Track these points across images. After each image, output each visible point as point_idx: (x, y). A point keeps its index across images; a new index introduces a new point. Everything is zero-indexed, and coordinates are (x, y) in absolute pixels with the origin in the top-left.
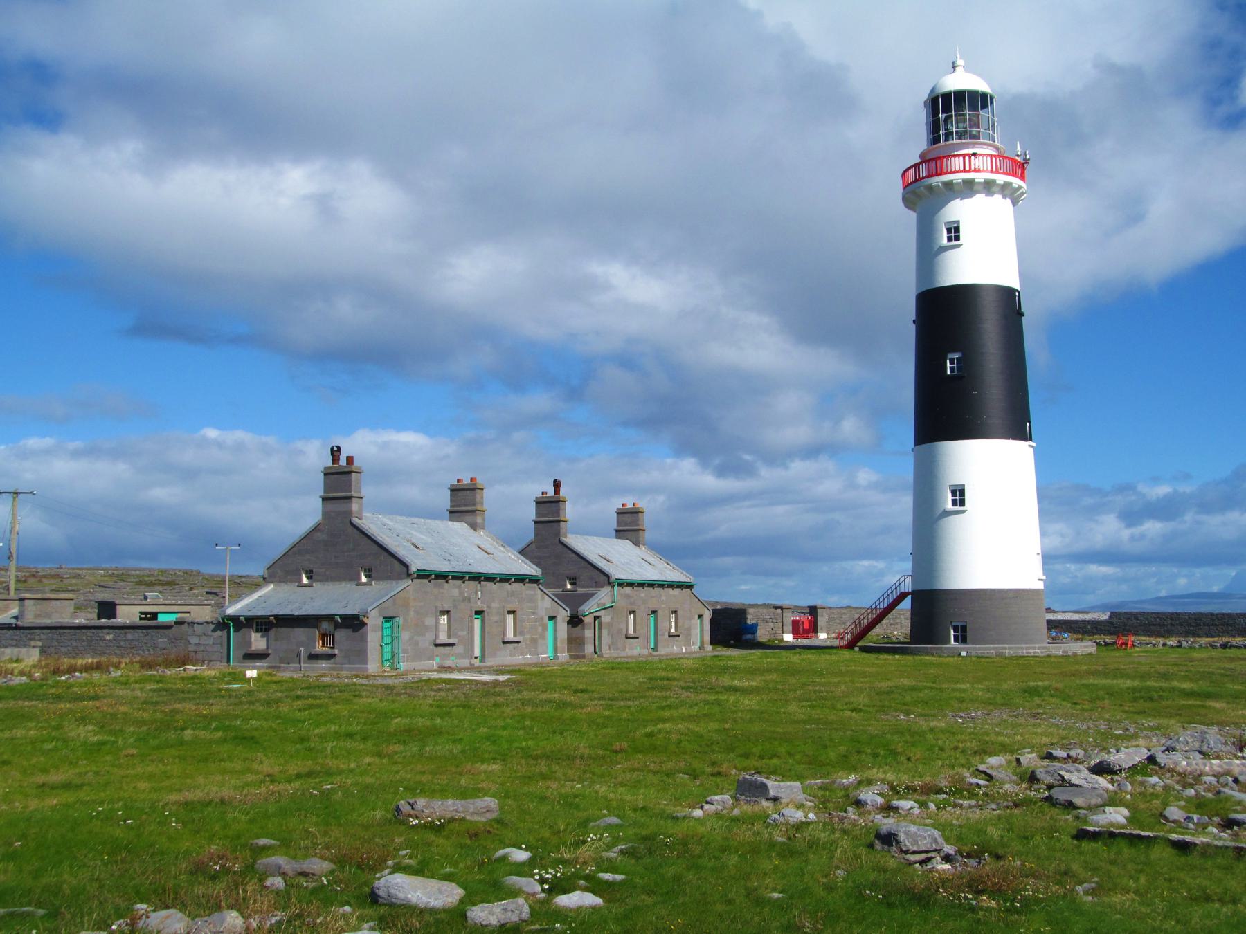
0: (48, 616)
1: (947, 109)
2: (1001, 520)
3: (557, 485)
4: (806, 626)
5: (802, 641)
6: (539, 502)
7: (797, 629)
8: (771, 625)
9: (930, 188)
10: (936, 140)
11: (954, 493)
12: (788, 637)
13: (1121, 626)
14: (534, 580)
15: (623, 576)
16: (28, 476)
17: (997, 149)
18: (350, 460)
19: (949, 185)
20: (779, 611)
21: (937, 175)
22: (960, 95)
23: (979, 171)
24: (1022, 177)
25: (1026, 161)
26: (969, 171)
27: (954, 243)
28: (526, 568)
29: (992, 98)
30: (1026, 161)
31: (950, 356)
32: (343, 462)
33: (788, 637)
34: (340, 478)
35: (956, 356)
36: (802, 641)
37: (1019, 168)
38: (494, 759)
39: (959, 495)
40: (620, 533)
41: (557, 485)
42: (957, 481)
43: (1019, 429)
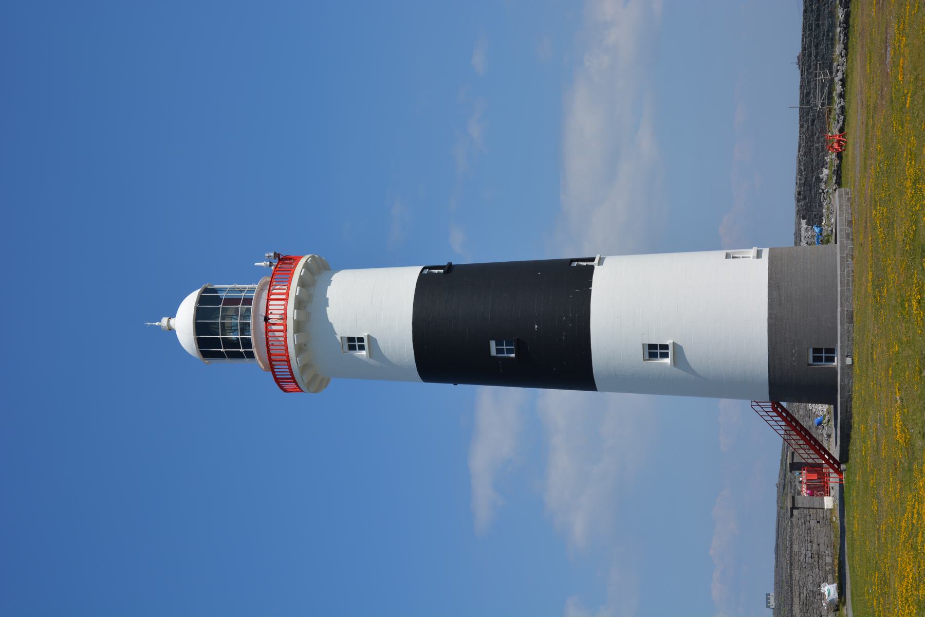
1: (216, 343)
2: (685, 296)
4: (814, 476)
8: (813, 523)
9: (304, 368)
11: (652, 356)
12: (829, 502)
13: (810, 206)
17: (262, 290)
19: (300, 349)
20: (795, 512)
21: (288, 361)
22: (200, 328)
23: (285, 314)
24: (296, 260)
25: (277, 255)
26: (285, 326)
27: (366, 343)
29: (206, 290)
30: (277, 255)
31: (493, 352)
33: (829, 502)
35: (493, 344)
37: (285, 262)
38: (880, 291)
39: (655, 351)
42: (638, 353)
43: (575, 278)
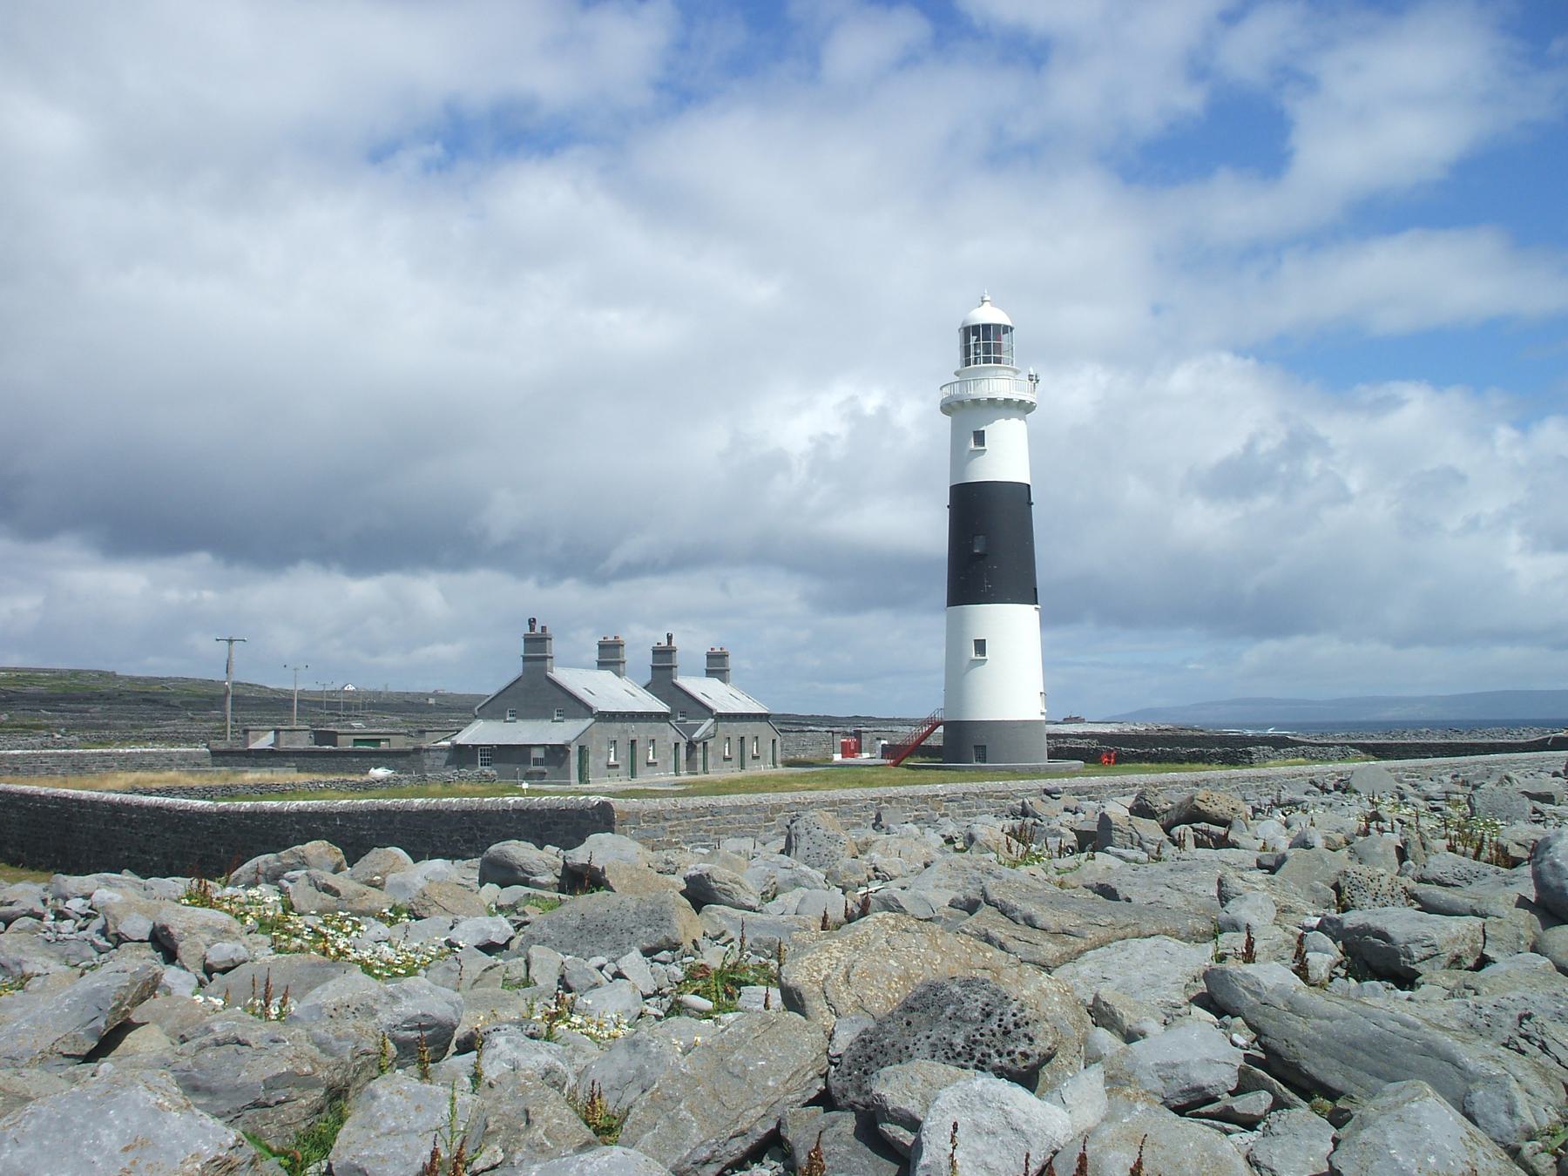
0: (293, 743)
3: (670, 638)
5: (849, 760)
6: (656, 652)
7: (846, 751)
10: (968, 363)
12: (838, 757)
14: (659, 717)
15: (720, 711)
16: (286, 641)
18: (544, 629)
22: (987, 327)
28: (660, 707)
32: (538, 630)
34: (537, 644)
36: (849, 760)
39: (980, 646)
40: (710, 673)
41: (670, 638)
43: (1028, 595)
